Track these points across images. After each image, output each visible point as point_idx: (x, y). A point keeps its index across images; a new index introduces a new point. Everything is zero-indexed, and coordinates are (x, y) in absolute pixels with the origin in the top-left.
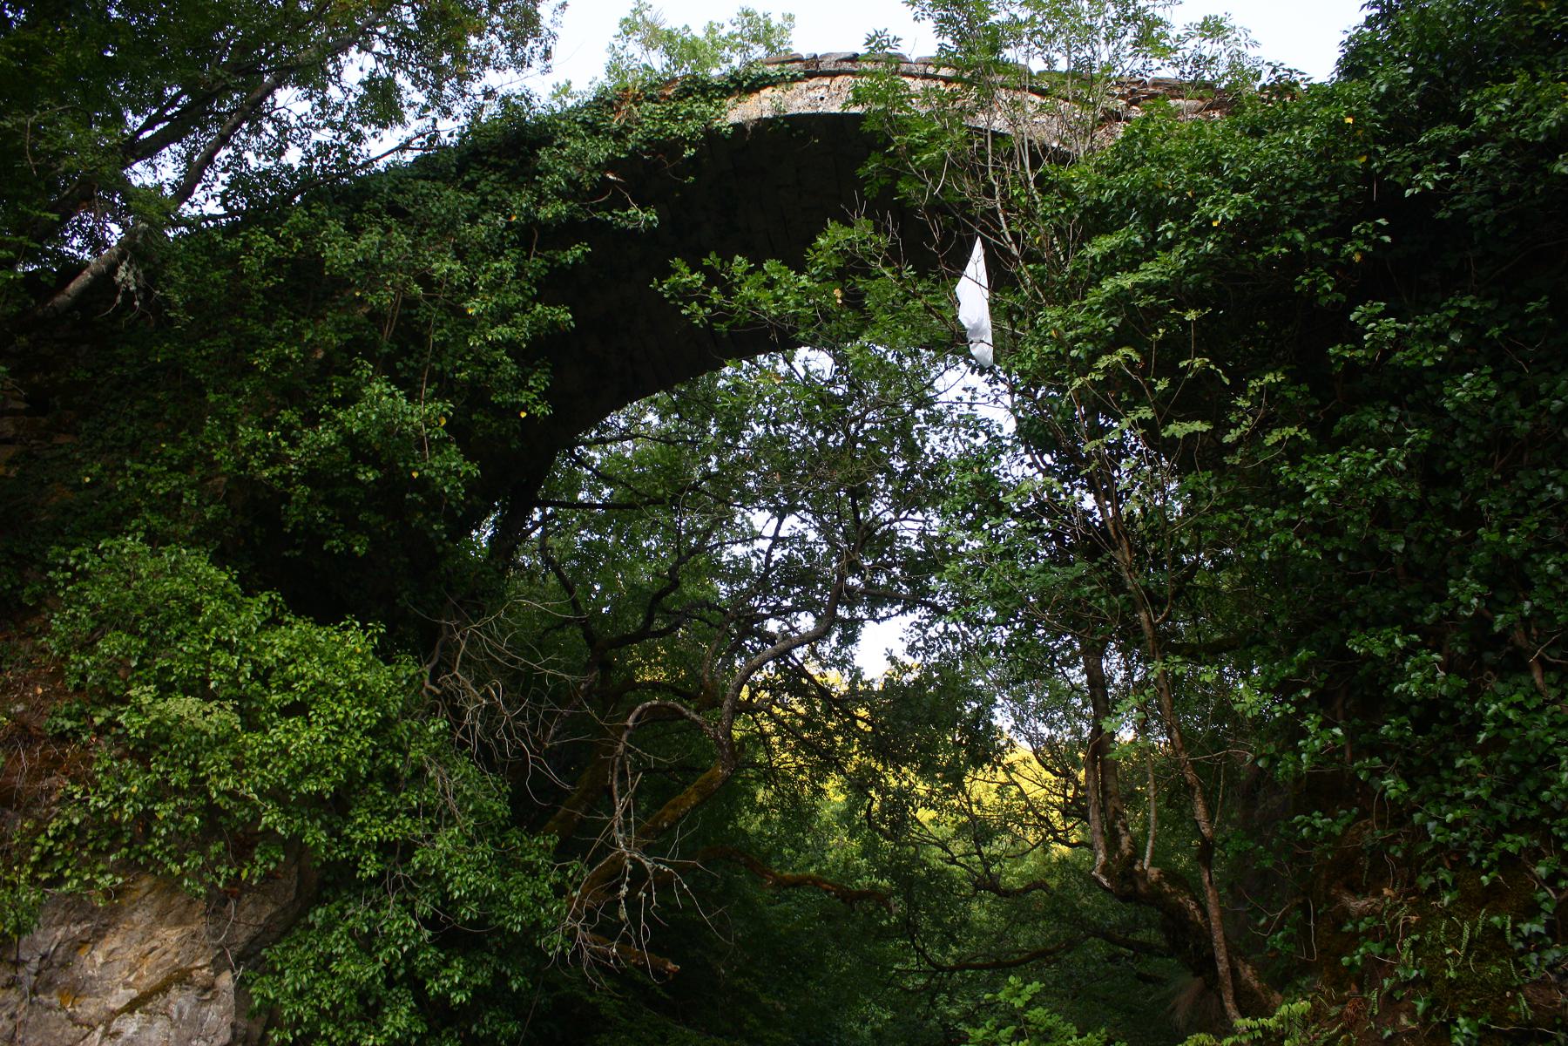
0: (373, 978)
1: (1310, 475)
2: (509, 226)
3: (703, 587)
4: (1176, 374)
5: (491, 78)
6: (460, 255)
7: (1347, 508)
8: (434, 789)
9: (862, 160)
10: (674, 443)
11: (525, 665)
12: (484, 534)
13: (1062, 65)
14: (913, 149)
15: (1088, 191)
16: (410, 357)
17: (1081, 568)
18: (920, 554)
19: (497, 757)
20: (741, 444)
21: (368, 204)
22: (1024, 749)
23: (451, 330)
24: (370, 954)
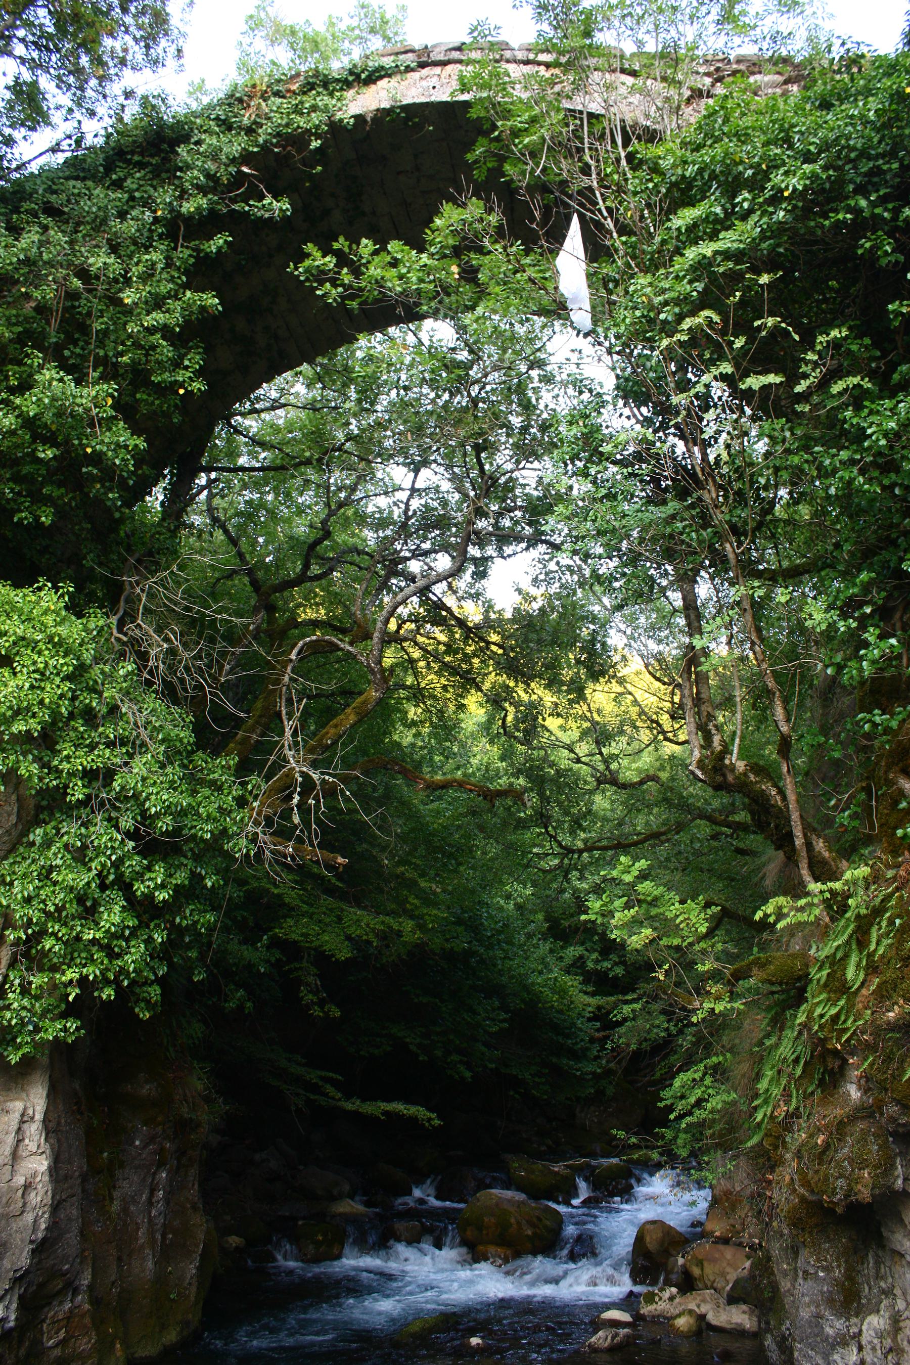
0: (88, 883)
1: (871, 419)
2: (156, 220)
3: (353, 535)
4: (752, 333)
5: (129, 79)
6: (114, 249)
7: (903, 448)
8: (127, 722)
9: (469, 146)
10: (318, 410)
11: (199, 611)
12: (157, 497)
13: (651, 47)
14: (516, 133)
15: (674, 166)
16: (76, 345)
17: (673, 506)
18: (539, 499)
19: (180, 693)
20: (379, 408)
21: (26, 206)
22: (636, 663)
23: (111, 319)
24: (85, 864)
